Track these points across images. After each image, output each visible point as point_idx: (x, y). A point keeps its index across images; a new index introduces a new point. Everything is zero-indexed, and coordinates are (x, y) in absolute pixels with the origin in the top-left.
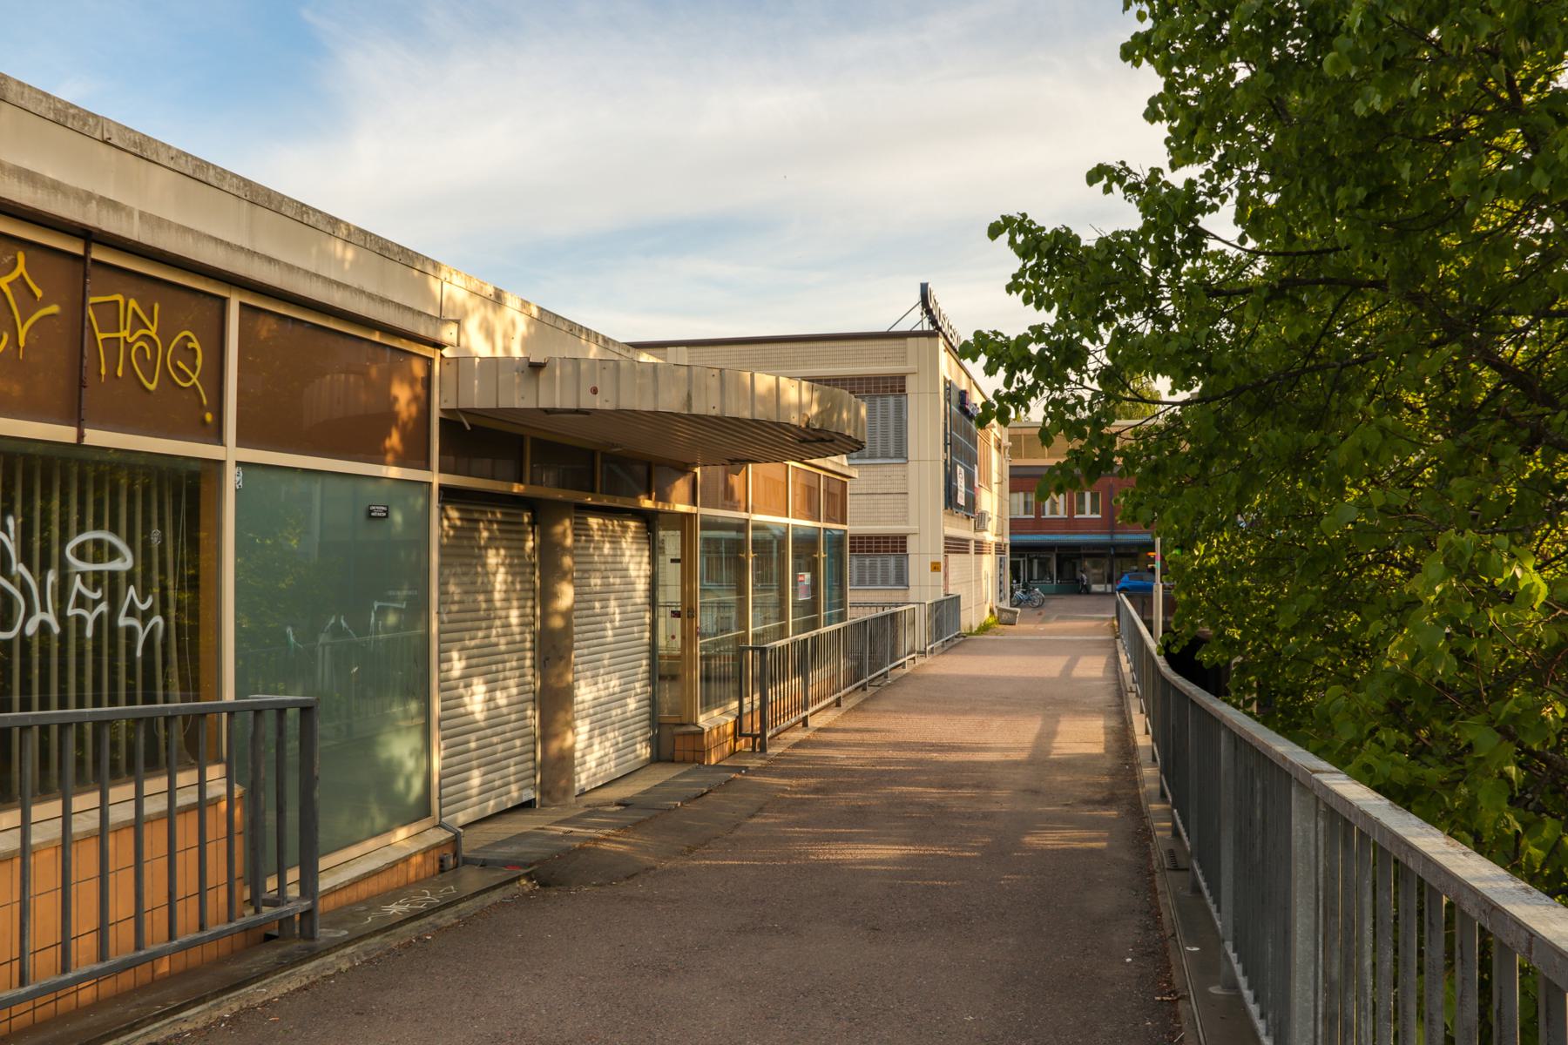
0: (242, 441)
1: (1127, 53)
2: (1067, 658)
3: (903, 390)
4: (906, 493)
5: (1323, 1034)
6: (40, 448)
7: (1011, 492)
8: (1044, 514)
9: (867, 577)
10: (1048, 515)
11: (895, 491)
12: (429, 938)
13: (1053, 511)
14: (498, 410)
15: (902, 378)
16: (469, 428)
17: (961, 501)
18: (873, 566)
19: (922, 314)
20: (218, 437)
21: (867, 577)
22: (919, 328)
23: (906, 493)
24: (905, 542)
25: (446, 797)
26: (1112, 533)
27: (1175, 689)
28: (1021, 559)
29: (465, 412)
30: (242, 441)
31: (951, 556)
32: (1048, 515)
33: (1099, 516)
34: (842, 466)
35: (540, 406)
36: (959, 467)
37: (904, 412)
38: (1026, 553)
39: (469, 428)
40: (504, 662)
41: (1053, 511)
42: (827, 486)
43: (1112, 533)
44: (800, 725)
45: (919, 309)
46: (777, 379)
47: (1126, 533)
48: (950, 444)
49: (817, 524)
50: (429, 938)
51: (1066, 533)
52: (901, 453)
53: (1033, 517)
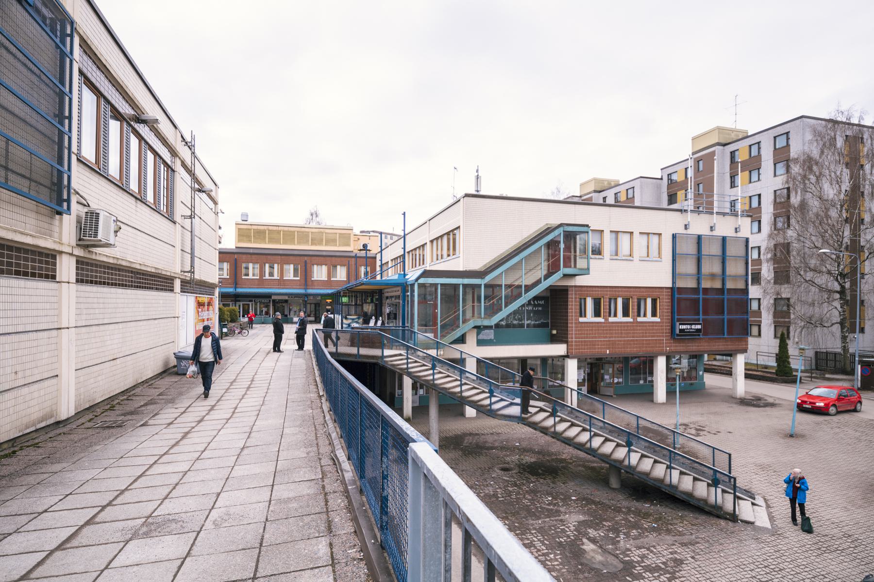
2: (467, 406)
5: (441, 518)
7: (219, 261)
8: (265, 276)
10: (267, 277)
12: (516, 524)
13: (271, 274)
26: (306, 289)
27: (341, 375)
28: (250, 303)
31: (350, 334)
32: (267, 277)
33: (298, 278)
38: (253, 299)
40: (353, 400)
41: (271, 274)
42: (633, 375)
43: (306, 289)
46: (366, 253)
47: (315, 289)
50: (516, 524)
51: (278, 288)
53: (258, 278)
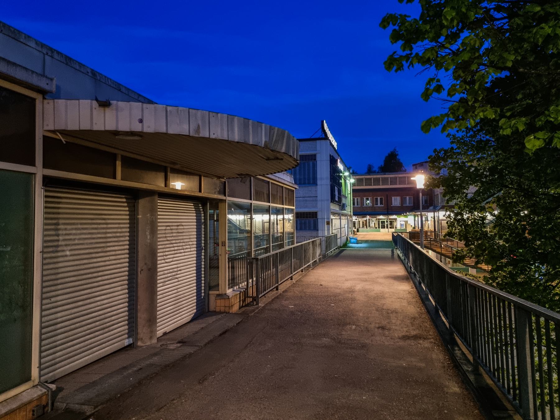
0: (45, 166)
1: (330, 156)
3: (315, 159)
4: (317, 197)
6: (180, 195)
9: (303, 227)
11: (312, 196)
14: (81, 131)
15: (315, 155)
16: (64, 143)
17: (337, 199)
18: (305, 223)
19: (322, 132)
20: (32, 163)
21: (303, 227)
22: (321, 137)
23: (317, 197)
24: (317, 214)
25: (44, 364)
29: (64, 132)
30: (45, 166)
34: (292, 183)
35: (107, 128)
36: (336, 187)
37: (316, 166)
39: (64, 143)
44: (275, 290)
45: (321, 130)
48: (333, 179)
49: (268, 204)
52: (315, 183)
53: (412, 205)
